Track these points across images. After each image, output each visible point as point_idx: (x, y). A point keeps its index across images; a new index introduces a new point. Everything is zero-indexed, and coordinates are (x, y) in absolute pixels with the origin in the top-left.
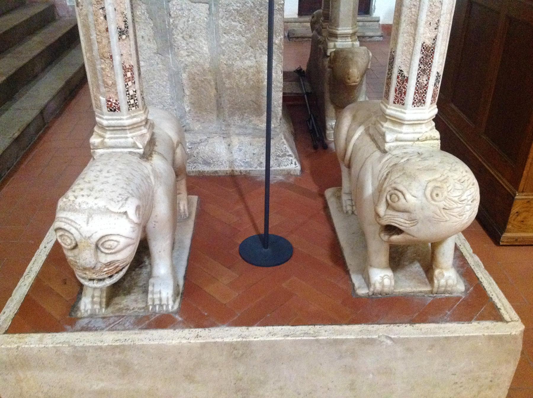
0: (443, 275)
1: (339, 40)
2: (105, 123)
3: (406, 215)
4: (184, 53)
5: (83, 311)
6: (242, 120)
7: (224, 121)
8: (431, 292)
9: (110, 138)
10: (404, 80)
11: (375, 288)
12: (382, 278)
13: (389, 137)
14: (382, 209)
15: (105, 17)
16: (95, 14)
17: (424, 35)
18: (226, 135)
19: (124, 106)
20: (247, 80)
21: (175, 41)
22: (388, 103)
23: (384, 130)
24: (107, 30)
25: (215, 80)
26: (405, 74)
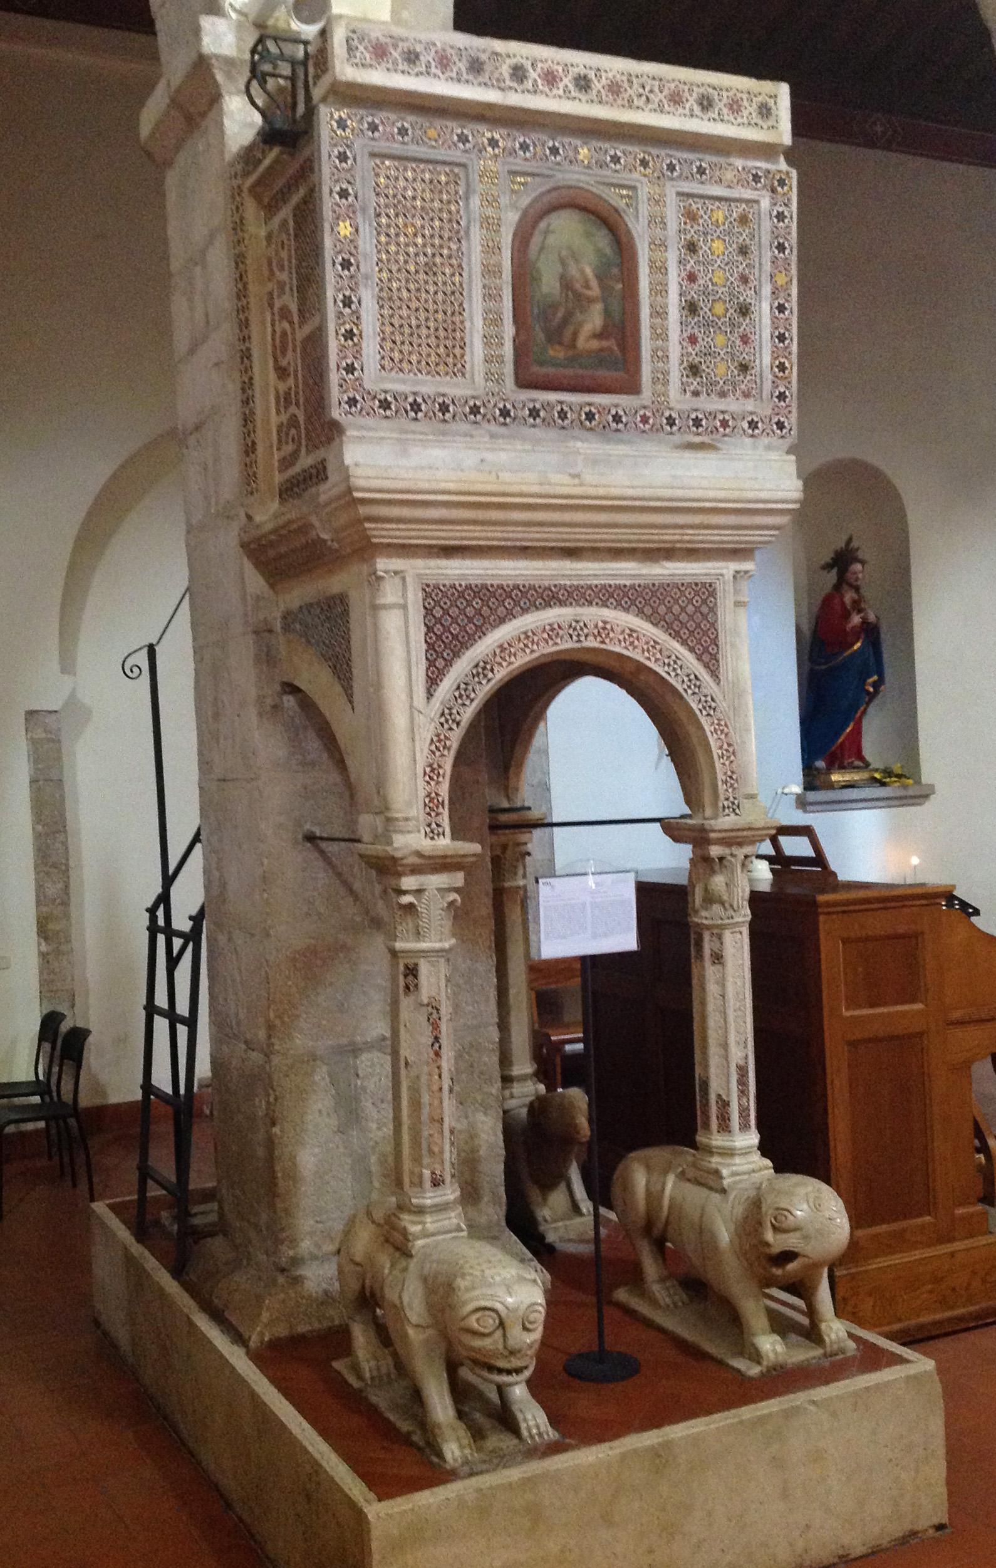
0: (831, 1328)
1: (515, 1084)
2: (428, 1202)
3: (798, 1234)
5: (451, 1461)
8: (825, 1355)
10: (724, 1104)
11: (768, 1360)
12: (770, 1345)
13: (725, 1172)
14: (769, 1236)
15: (440, 1077)
21: (363, 1111)
22: (711, 1134)
23: (714, 1166)
24: (441, 1089)
26: (724, 1097)
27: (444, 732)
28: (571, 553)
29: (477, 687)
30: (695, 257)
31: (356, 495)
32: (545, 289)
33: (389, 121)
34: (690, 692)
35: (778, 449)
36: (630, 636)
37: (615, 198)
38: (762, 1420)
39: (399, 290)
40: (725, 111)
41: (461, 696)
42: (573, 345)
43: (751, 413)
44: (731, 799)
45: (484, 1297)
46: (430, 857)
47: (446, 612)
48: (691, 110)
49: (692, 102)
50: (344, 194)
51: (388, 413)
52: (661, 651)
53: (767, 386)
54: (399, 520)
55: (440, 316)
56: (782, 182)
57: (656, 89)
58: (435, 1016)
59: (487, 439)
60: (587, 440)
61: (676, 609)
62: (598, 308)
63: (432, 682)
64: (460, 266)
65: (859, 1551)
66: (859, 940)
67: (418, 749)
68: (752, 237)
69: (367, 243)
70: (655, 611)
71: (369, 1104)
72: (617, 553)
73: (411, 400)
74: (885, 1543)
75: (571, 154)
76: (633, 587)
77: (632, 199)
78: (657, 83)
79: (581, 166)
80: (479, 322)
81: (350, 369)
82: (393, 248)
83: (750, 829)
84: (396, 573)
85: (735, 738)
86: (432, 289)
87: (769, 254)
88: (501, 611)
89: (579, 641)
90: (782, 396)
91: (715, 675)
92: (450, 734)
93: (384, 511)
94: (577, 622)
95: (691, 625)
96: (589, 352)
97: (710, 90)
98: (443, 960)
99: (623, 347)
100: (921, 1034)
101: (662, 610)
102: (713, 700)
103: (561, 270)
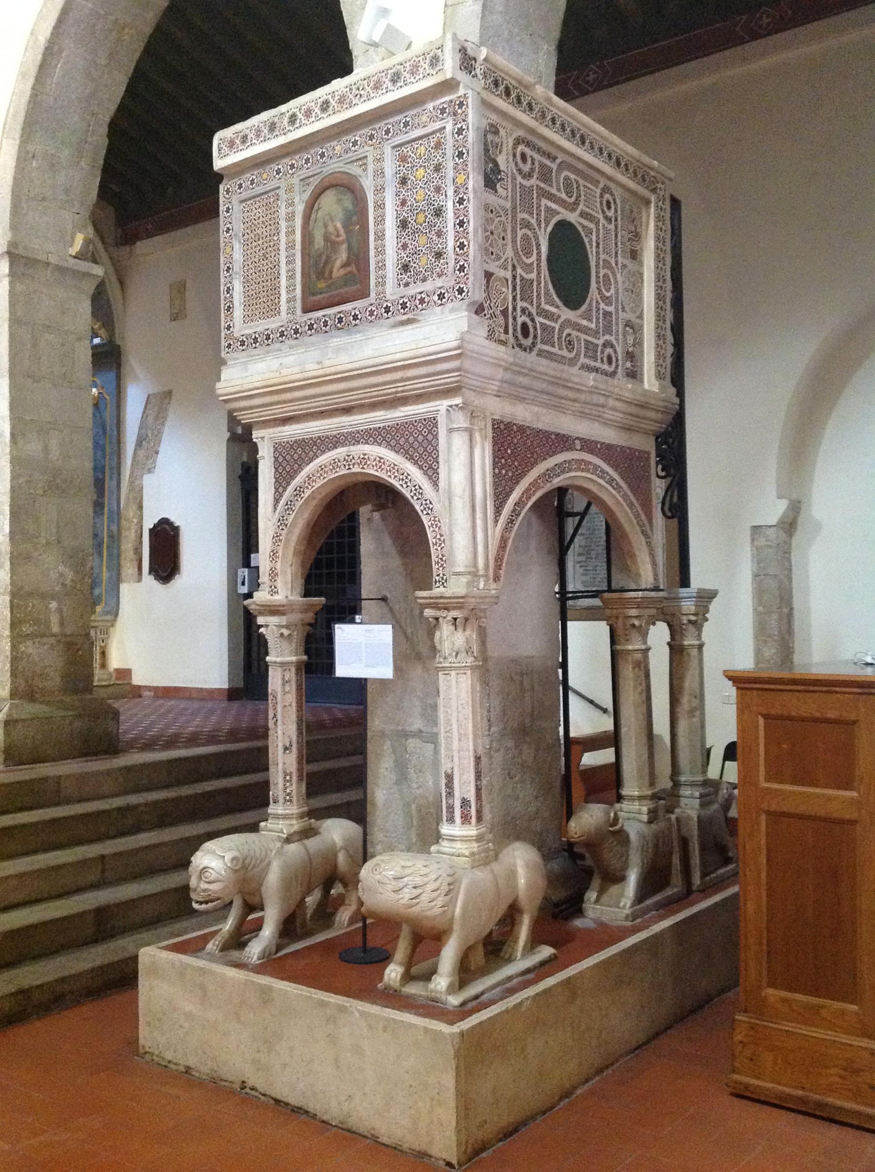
19: (281, 800)
28: (347, 410)
32: (316, 247)
34: (415, 498)
38: (323, 1004)
40: (408, 76)
44: (441, 575)
46: (263, 606)
53: (452, 263)
54: (251, 408)
62: (344, 246)
65: (385, 1140)
66: (781, 718)
71: (412, 771)
72: (374, 406)
74: (405, 1147)
76: (384, 428)
91: (435, 484)
102: (431, 503)
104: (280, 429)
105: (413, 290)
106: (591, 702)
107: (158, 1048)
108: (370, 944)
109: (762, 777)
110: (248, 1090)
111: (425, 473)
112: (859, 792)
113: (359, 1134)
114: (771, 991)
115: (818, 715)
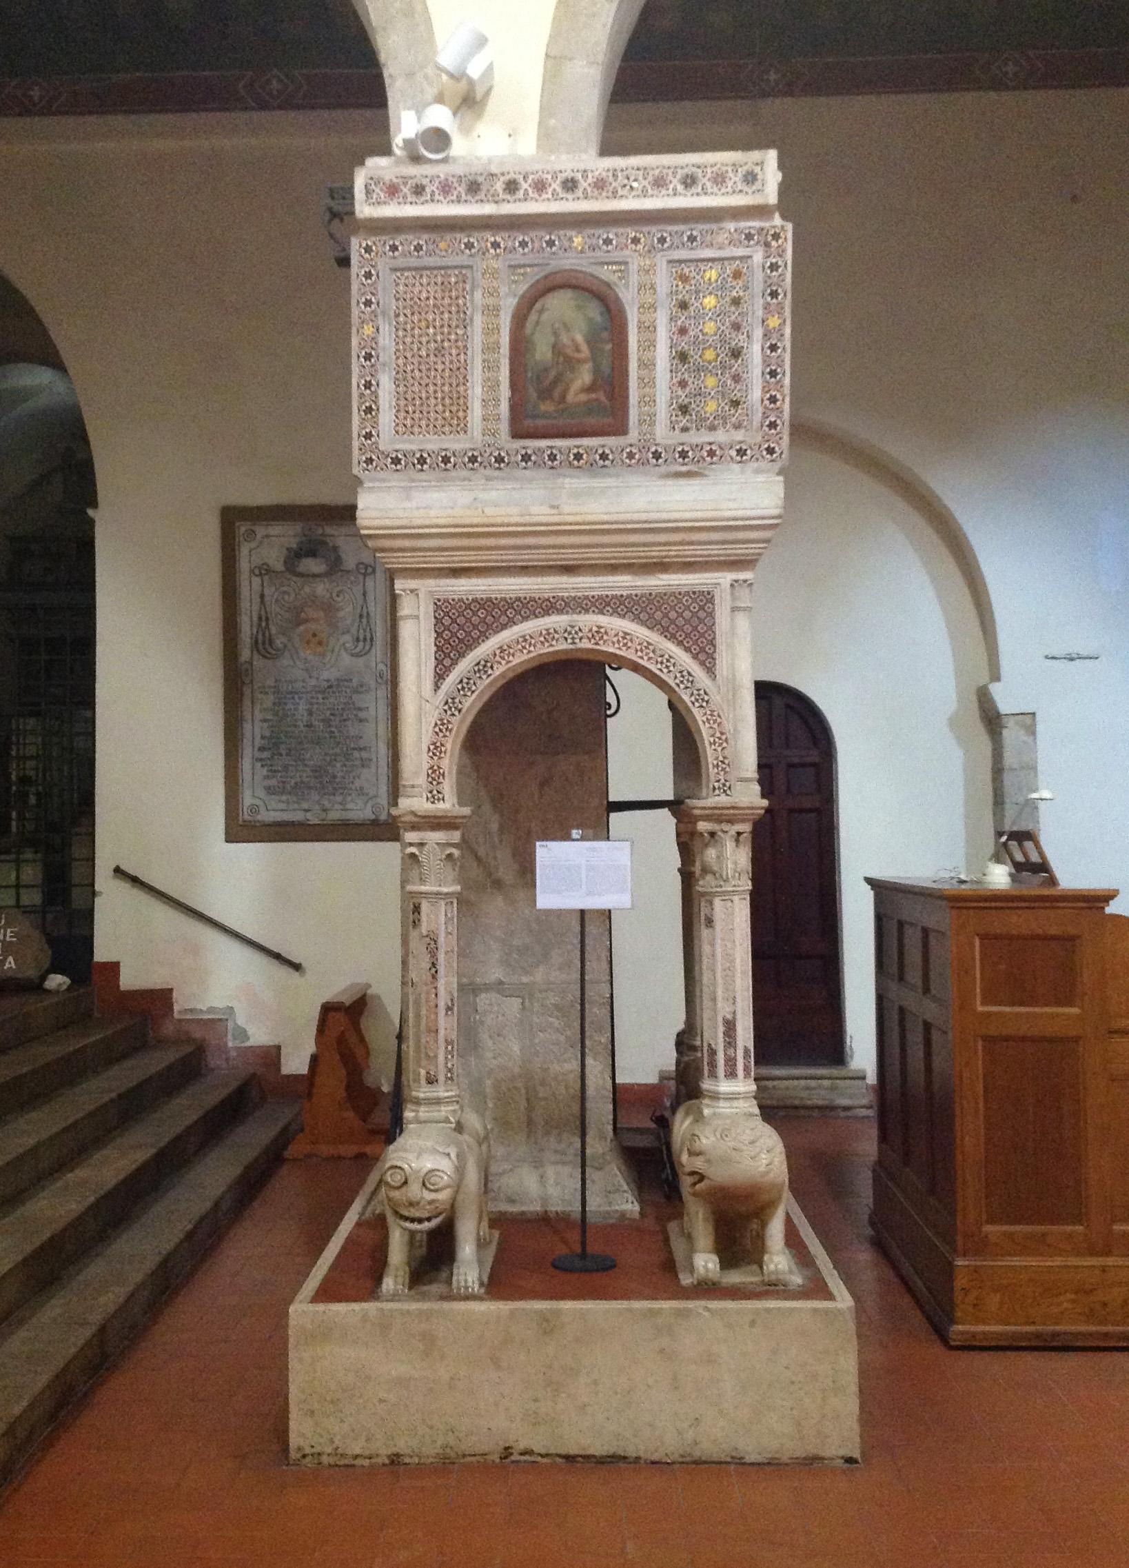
2: (422, 1095)
3: (701, 1158)
4: (489, 1055)
6: (560, 1142)
7: (536, 1143)
9: (424, 1113)
10: (713, 1053)
16: (428, 993)
17: (724, 1010)
18: (538, 1164)
20: (567, 1088)
25: (527, 1088)
27: (446, 717)
28: (569, 570)
29: (478, 682)
30: (686, 314)
31: (363, 532)
32: (538, 356)
33: (407, 242)
35: (768, 471)
36: (624, 638)
37: (606, 273)
38: (652, 1313)
39: (412, 371)
40: (709, 184)
41: (463, 688)
42: (563, 398)
43: (741, 442)
45: (402, 1159)
46: (425, 817)
47: (454, 621)
48: (675, 189)
49: (676, 183)
50: (368, 303)
51: (399, 467)
52: (654, 651)
53: (758, 417)
55: (446, 388)
56: (776, 236)
57: (641, 178)
58: (433, 946)
59: (483, 481)
60: (578, 478)
61: (673, 615)
63: (440, 677)
64: (465, 347)
67: (424, 731)
68: (746, 288)
69: (387, 340)
70: (651, 617)
71: (486, 1036)
72: (614, 569)
73: (418, 455)
74: (785, 1459)
75: (566, 244)
76: (629, 596)
77: (624, 275)
78: (641, 173)
79: (576, 251)
80: (478, 390)
81: (368, 436)
82: (408, 340)
83: (733, 808)
84: (412, 591)
85: (728, 727)
86: (440, 367)
87: (761, 301)
88: (504, 619)
89: (574, 643)
90: (773, 425)
91: (711, 671)
92: (453, 719)
93: (387, 543)
94: (573, 627)
95: (688, 628)
96: (578, 405)
97: (694, 169)
98: (443, 903)
99: (611, 397)
100: (1076, 1040)
101: (658, 615)
103: (553, 339)
104: (448, 581)
105: (694, 438)
106: (277, 957)
107: (332, 1441)
108: (589, 1250)
109: (978, 1003)
110: (515, 1457)
111: (695, 657)
112: (1082, 1008)
113: (714, 1462)
114: (988, 1228)
115: (1040, 931)
